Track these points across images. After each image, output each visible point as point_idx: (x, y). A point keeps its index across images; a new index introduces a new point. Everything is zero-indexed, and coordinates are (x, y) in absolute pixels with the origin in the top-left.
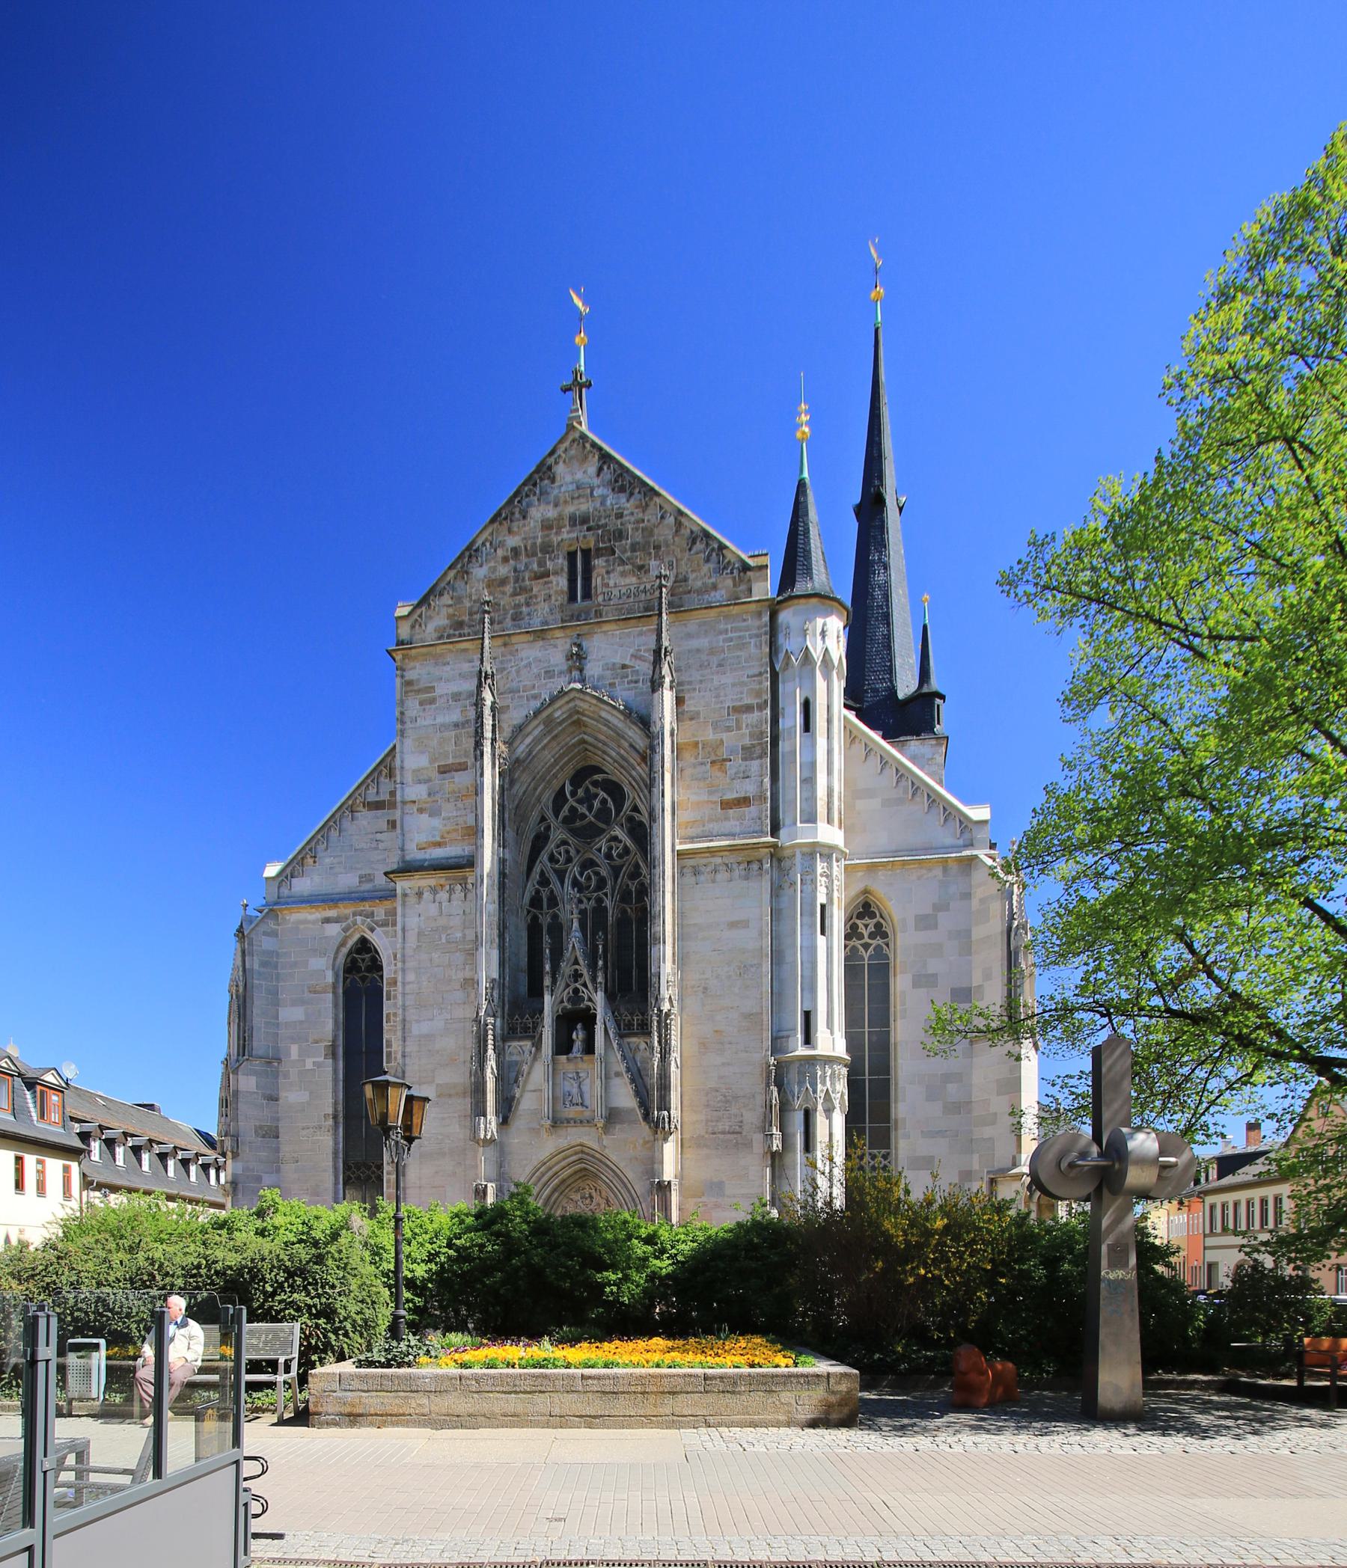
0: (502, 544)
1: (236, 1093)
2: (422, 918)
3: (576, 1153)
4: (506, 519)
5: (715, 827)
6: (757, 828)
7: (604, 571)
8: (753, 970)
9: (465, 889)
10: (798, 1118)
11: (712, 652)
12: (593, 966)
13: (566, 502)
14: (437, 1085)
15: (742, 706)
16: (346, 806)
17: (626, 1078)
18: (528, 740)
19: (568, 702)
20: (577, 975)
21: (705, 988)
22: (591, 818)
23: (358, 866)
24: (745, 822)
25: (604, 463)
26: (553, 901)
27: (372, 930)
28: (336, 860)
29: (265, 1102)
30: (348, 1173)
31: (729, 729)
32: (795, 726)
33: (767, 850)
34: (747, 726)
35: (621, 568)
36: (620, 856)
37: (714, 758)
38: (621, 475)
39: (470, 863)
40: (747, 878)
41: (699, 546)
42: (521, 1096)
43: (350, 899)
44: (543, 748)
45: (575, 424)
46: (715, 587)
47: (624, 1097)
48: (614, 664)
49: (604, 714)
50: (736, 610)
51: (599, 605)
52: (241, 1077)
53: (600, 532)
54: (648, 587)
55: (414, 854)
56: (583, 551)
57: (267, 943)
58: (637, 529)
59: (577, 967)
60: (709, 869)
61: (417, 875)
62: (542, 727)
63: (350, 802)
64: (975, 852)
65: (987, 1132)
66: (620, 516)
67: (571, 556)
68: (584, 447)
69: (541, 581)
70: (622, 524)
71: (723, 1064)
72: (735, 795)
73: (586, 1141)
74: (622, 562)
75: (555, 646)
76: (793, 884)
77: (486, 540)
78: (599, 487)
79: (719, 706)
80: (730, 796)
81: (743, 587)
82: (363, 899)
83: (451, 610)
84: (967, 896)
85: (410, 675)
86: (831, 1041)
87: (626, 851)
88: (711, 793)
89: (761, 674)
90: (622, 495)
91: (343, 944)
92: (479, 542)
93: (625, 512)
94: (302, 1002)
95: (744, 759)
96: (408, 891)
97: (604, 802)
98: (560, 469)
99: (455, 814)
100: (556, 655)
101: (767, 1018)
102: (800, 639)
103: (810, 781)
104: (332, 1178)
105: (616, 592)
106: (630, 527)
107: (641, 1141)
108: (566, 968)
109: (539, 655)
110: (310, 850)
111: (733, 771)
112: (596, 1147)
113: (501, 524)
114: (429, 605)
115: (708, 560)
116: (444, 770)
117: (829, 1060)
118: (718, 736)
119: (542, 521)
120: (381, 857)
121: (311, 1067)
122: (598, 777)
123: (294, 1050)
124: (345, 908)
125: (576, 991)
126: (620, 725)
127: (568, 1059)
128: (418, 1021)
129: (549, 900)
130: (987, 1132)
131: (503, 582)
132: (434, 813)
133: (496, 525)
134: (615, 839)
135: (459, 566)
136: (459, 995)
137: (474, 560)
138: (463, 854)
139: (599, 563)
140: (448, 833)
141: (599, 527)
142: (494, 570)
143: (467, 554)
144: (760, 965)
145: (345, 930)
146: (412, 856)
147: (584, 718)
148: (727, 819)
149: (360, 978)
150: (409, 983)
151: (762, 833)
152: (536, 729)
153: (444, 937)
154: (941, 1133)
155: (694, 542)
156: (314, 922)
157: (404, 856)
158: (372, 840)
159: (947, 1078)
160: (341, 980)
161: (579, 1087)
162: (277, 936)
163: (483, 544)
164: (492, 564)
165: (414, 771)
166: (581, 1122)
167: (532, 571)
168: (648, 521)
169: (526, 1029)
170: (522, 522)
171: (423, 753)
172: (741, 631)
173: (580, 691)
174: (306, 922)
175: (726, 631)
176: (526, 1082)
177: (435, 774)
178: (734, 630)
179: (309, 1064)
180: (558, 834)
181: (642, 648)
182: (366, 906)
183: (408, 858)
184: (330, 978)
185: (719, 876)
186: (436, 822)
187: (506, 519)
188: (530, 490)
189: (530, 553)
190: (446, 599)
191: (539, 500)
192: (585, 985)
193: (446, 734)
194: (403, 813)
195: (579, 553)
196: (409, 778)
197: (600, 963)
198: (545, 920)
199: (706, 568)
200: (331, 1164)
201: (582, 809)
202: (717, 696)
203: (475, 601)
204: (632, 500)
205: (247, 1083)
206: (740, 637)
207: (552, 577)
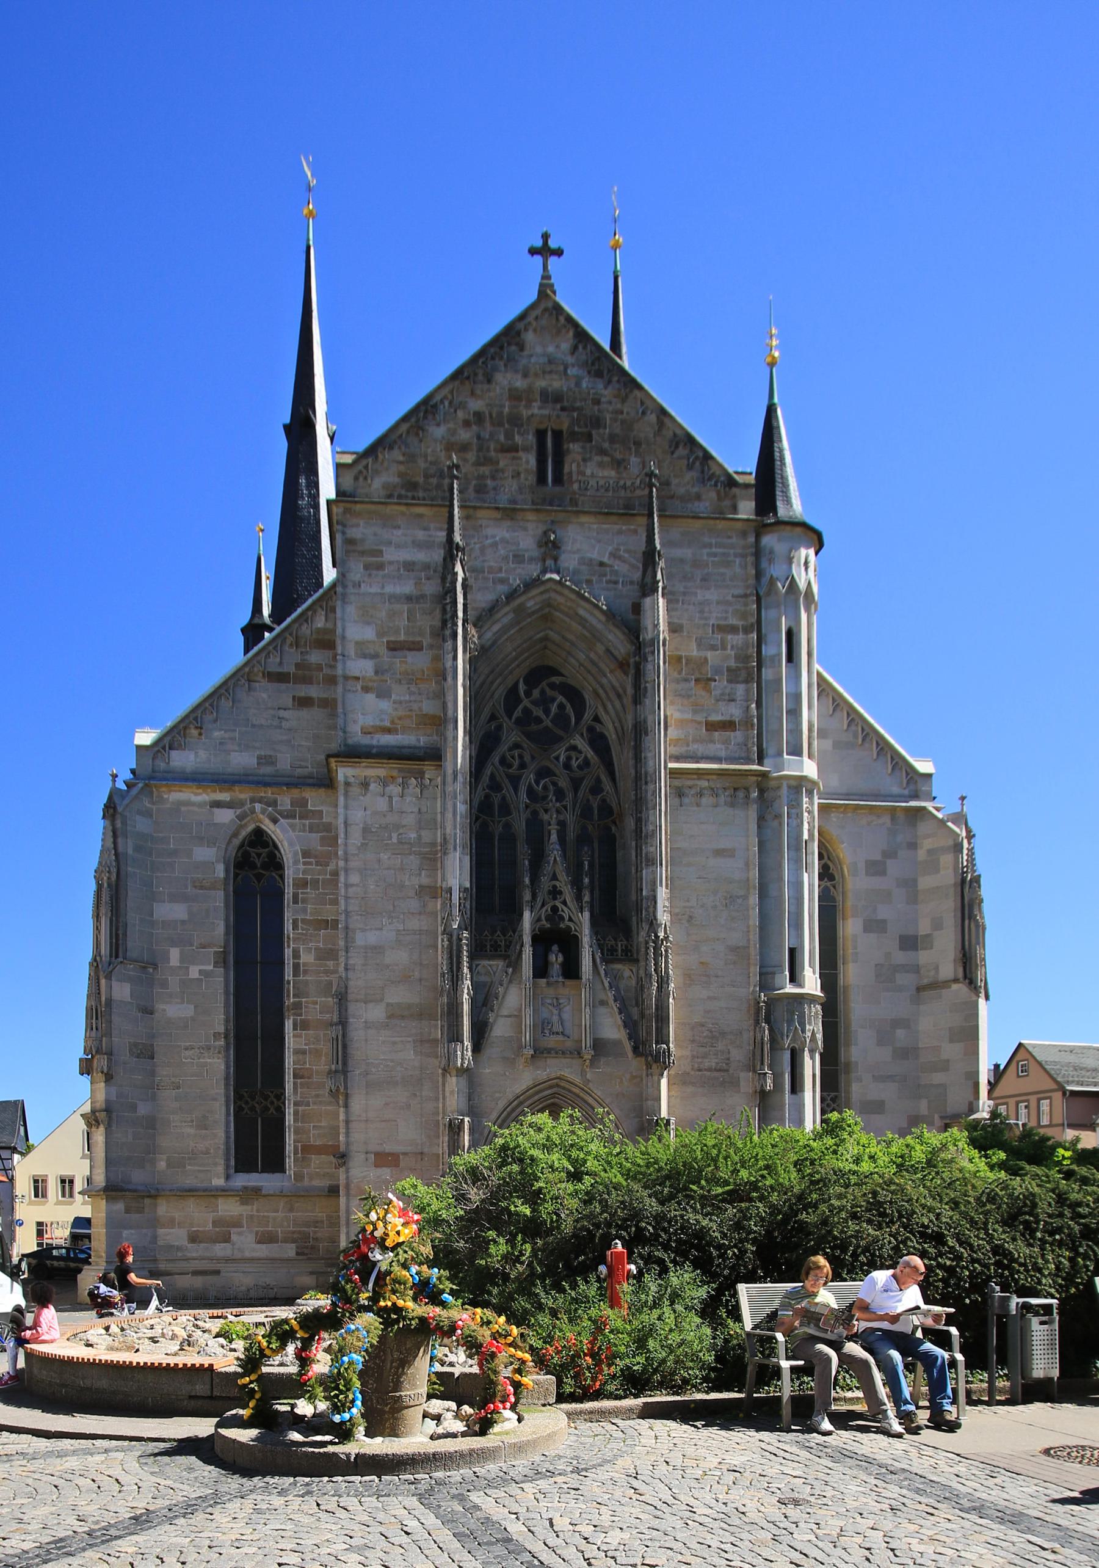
0: (463, 405)
1: (109, 1002)
2: (368, 812)
3: (551, 1087)
4: (468, 378)
5: (699, 749)
6: (743, 755)
7: (579, 458)
8: (739, 901)
9: (423, 787)
10: (787, 1056)
11: (696, 564)
12: (577, 884)
13: (536, 375)
14: (388, 1004)
15: (727, 626)
16: (242, 673)
17: (615, 1007)
18: (496, 628)
19: (542, 593)
20: (555, 893)
21: (691, 917)
22: (547, 722)
23: (257, 745)
24: (731, 747)
25: (580, 342)
26: (505, 809)
27: (275, 821)
28: (227, 735)
29: (139, 1015)
30: (239, 1103)
31: (713, 648)
32: (780, 654)
33: (755, 778)
34: (732, 647)
35: (598, 458)
36: (580, 767)
37: (698, 676)
38: (598, 359)
39: (435, 755)
40: (732, 805)
41: (682, 451)
42: (495, 1021)
43: (249, 782)
45: (549, 292)
46: (698, 497)
47: (612, 1028)
48: (591, 560)
49: (581, 612)
50: (721, 525)
51: (574, 493)
52: (115, 984)
53: (575, 414)
54: (629, 483)
55: (357, 737)
56: (553, 431)
57: (141, 825)
58: (616, 420)
59: (554, 882)
60: (693, 792)
61: (365, 762)
62: (511, 616)
63: (247, 670)
64: (923, 804)
65: (938, 1078)
66: (597, 402)
67: (541, 435)
68: (557, 319)
69: (509, 455)
70: (599, 410)
71: (709, 998)
72: (719, 718)
73: (567, 1073)
74: (602, 452)
75: (525, 529)
76: (778, 816)
77: (445, 397)
78: (573, 366)
79: (702, 622)
80: (715, 718)
81: (727, 503)
82: (267, 784)
83: (402, 468)
84: (913, 846)
85: (354, 533)
86: (812, 983)
87: (587, 763)
88: (695, 712)
89: (746, 596)
90: (598, 380)
91: (235, 835)
92: (438, 398)
93: (603, 400)
94: (184, 898)
96: (352, 780)
97: (561, 707)
98: (529, 337)
99: (407, 698)
100: (527, 541)
101: (754, 952)
102: (785, 567)
103: (795, 713)
104: (224, 1109)
105: (593, 482)
106: (608, 416)
107: (628, 1076)
108: (545, 883)
109: (507, 535)
110: (196, 719)
111: (718, 692)
112: (578, 1080)
113: (462, 383)
114: (377, 457)
115: (690, 467)
116: (394, 647)
117: (811, 999)
118: (702, 654)
119: (510, 390)
120: (285, 738)
121: (197, 976)
122: (556, 680)
123: (175, 955)
124: (241, 792)
125: (555, 909)
126: (599, 626)
127: (548, 984)
128: (363, 930)
130: (938, 1078)
131: (464, 448)
132: (383, 694)
133: (457, 383)
134: (574, 748)
135: (413, 420)
136: (414, 904)
137: (430, 417)
138: (417, 744)
139: (575, 448)
140: (400, 718)
141: (574, 409)
142: (453, 432)
143: (423, 408)
144: (745, 897)
145: (241, 817)
146: (355, 739)
147: (558, 614)
148: (712, 741)
149: (254, 875)
150: (352, 885)
151: (749, 761)
152: (505, 617)
153: (395, 836)
154: (890, 1078)
155: (677, 447)
156: (201, 805)
157: (345, 739)
158: (274, 716)
159: (897, 1023)
160: (232, 875)
161: (559, 1015)
162: (151, 816)
163: (442, 401)
164: (451, 425)
165: (357, 643)
166: (563, 1053)
168: (628, 413)
169: (496, 947)
170: (486, 386)
171: (368, 623)
173: (560, 582)
174: (188, 803)
175: (710, 546)
176: (500, 1005)
177: (383, 651)
178: (717, 545)
179: (194, 972)
180: (511, 736)
182: (268, 793)
183: (350, 742)
184: (220, 871)
185: (704, 801)
186: (385, 705)
187: (468, 378)
188: (495, 353)
190: (397, 454)
191: (505, 365)
192: (564, 903)
193: (397, 607)
194: (344, 689)
195: (549, 433)
196: (351, 650)
197: (586, 880)
198: (498, 829)
199: (689, 476)
200: (222, 1091)
201: (538, 712)
202: (701, 612)
203: (431, 463)
204: (610, 388)
205: (122, 991)
206: (724, 554)
207: (521, 454)
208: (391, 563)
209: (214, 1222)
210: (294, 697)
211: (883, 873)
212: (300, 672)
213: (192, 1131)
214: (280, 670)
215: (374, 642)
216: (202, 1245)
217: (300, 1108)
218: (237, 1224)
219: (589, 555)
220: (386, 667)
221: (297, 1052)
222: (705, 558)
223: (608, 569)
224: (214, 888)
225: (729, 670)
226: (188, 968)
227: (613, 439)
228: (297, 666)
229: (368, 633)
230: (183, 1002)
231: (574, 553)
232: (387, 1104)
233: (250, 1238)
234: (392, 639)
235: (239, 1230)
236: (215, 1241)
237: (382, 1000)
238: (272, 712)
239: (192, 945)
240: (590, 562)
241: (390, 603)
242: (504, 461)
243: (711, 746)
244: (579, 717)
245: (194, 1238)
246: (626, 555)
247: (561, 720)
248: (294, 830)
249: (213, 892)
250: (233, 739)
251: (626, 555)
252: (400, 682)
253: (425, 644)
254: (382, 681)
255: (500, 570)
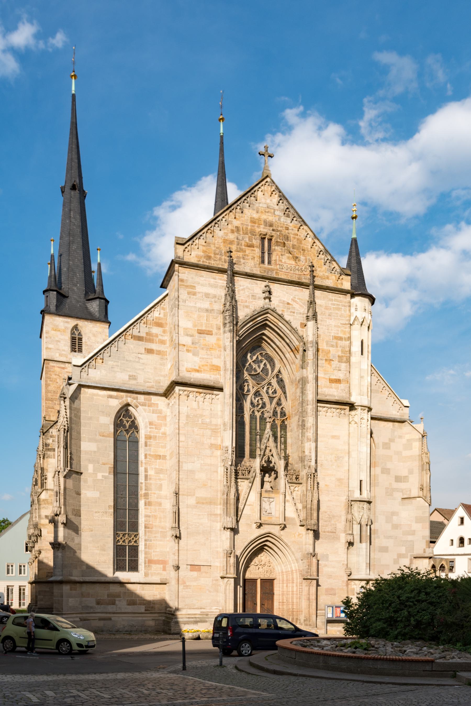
2: (189, 408)
14: (197, 497)
15: (338, 337)
24: (339, 391)
28: (115, 364)
31: (332, 346)
44: (233, 329)
46: (328, 278)
48: (284, 301)
58: (295, 238)
66: (287, 229)
71: (329, 501)
80: (333, 377)
83: (204, 248)
93: (290, 228)
94: (96, 441)
95: (339, 362)
105: (285, 265)
106: (292, 236)
109: (249, 286)
111: (334, 366)
116: (200, 332)
119: (251, 218)
129: (281, 413)
140: (203, 366)
141: (278, 231)
142: (226, 234)
148: (331, 388)
150: (181, 441)
153: (200, 420)
158: (136, 357)
165: (184, 329)
167: (245, 241)
170: (241, 215)
172: (338, 302)
175: (332, 300)
179: (100, 476)
181: (297, 297)
186: (196, 359)
189: (245, 232)
201: (255, 366)
203: (217, 248)
206: (338, 304)
208: (199, 293)
209: (108, 595)
210: (145, 348)
211: (389, 448)
212: (148, 337)
213: (98, 552)
214: (139, 335)
215: (192, 329)
216: (102, 606)
217: (148, 543)
218: (119, 596)
219: (283, 299)
220: (197, 341)
221: (146, 516)
222: (330, 305)
223: (291, 306)
224: (109, 437)
225: (339, 356)
226: (96, 474)
227: (294, 246)
228: (147, 333)
229: (189, 325)
230: (94, 490)
231: (277, 297)
232: (195, 543)
233: (125, 603)
234: (200, 328)
235: (119, 599)
236: (108, 604)
237: (194, 495)
238: (135, 355)
239: (98, 463)
240: (283, 302)
241: (199, 312)
242: (248, 251)
243: (331, 390)
244: (273, 370)
245: (98, 603)
246: (298, 301)
247: (265, 370)
248: (145, 412)
249: (108, 438)
250: (117, 366)
251: (298, 301)
252: (203, 349)
253: (214, 333)
254: (195, 348)
255: (246, 301)
